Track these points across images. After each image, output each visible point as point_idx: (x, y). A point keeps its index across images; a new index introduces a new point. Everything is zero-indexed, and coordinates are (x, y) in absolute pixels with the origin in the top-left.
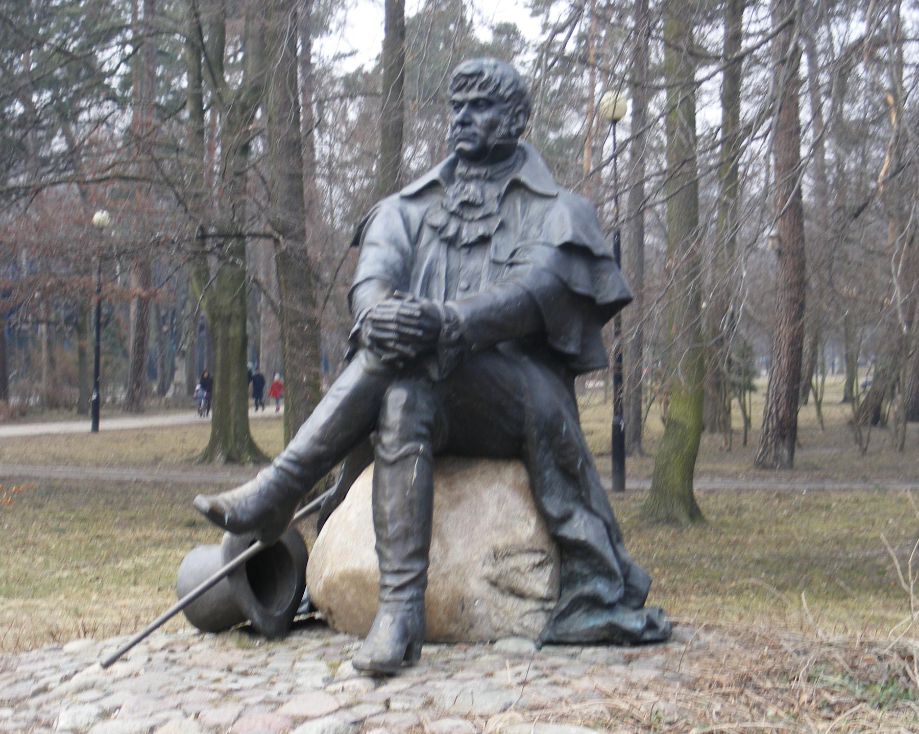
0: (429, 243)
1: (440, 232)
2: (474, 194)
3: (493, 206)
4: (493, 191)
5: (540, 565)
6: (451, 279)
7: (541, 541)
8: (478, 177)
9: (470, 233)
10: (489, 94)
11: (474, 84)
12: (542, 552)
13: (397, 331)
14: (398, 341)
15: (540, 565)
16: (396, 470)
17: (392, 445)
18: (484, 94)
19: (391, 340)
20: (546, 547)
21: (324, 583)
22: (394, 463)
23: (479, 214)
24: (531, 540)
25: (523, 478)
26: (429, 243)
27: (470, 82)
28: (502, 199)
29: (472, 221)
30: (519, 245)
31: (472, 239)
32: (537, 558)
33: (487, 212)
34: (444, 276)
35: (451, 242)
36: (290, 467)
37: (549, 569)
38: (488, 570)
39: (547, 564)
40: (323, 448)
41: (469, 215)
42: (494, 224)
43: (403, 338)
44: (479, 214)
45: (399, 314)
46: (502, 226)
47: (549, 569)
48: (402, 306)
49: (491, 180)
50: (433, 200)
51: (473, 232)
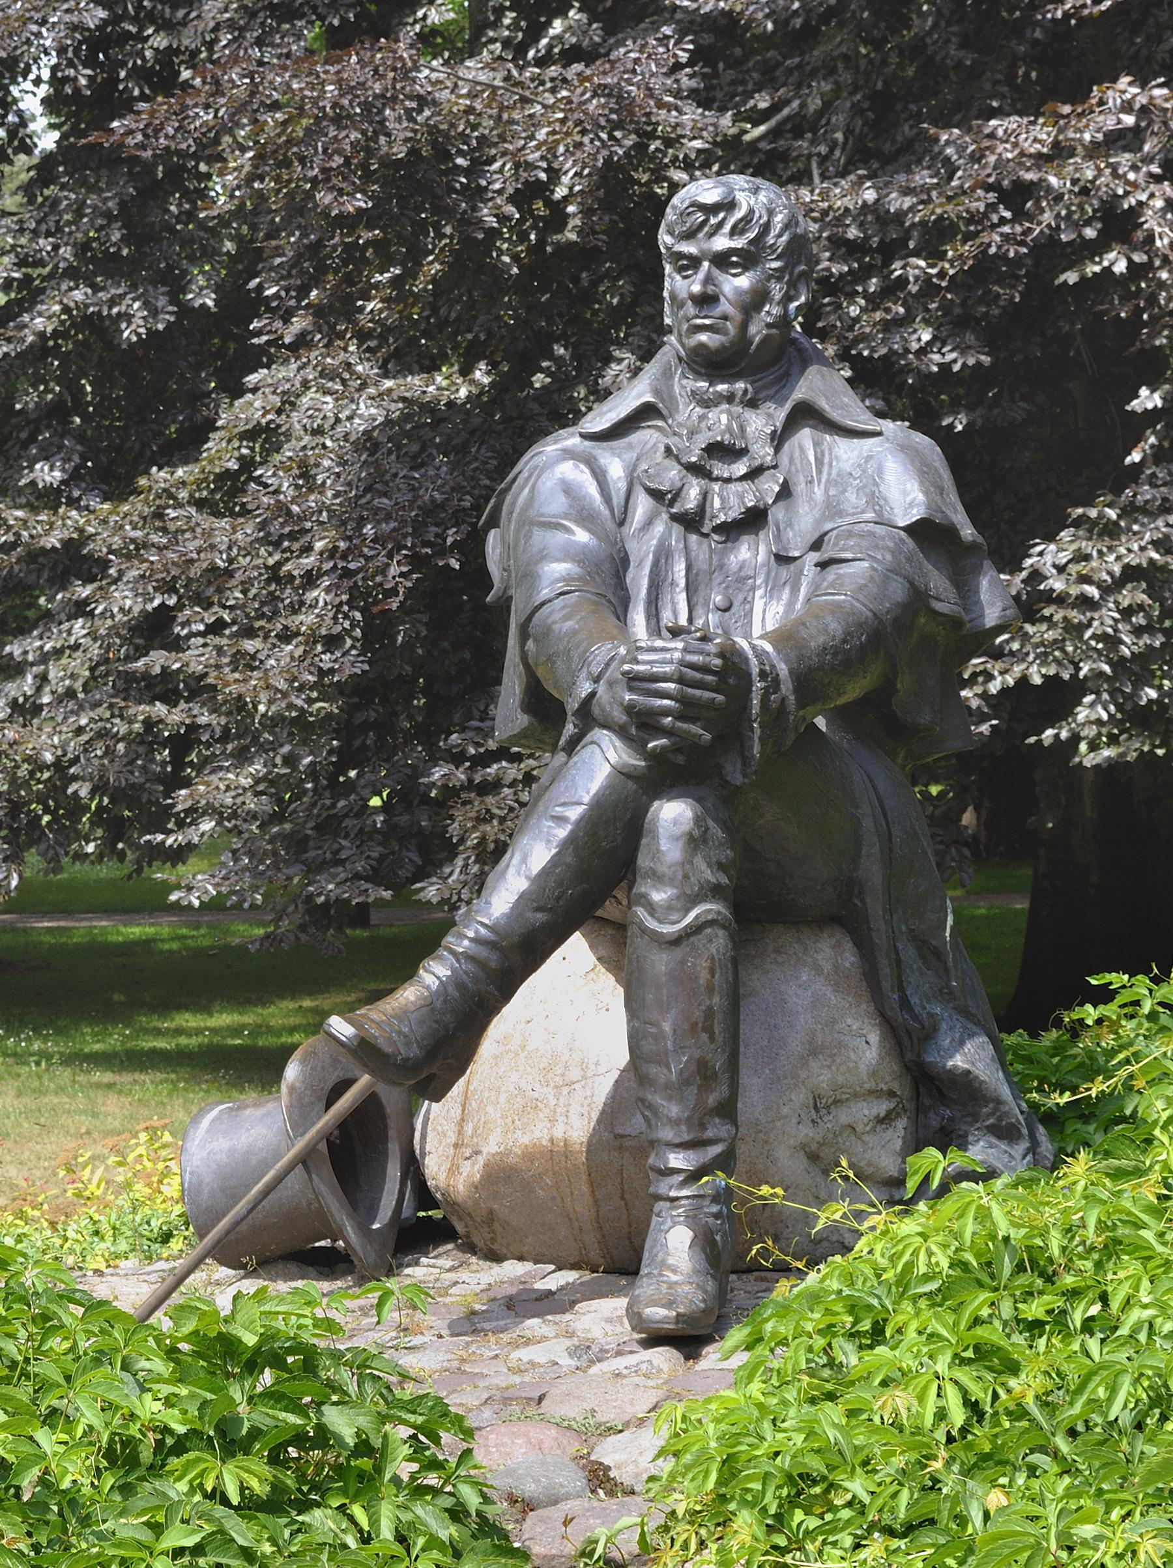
0: (649, 523)
1: (671, 504)
2: (729, 429)
3: (763, 452)
4: (759, 424)
5: (885, 1120)
6: (696, 590)
7: (891, 1077)
8: (730, 398)
9: (728, 502)
10: (751, 242)
11: (721, 225)
12: (891, 1094)
13: (680, 698)
14: (680, 717)
15: (885, 1120)
16: (678, 952)
17: (669, 908)
18: (739, 243)
19: (666, 712)
20: (896, 1086)
21: (486, 1165)
22: (676, 941)
23: (740, 468)
24: (873, 1074)
25: (849, 958)
26: (649, 523)
27: (713, 221)
28: (779, 439)
29: (728, 480)
30: (829, 526)
31: (734, 514)
32: (882, 1107)
33: (757, 463)
34: (682, 583)
35: (691, 522)
36: (483, 952)
37: (901, 1124)
38: (806, 1132)
39: (898, 1115)
40: (541, 917)
41: (720, 469)
42: (770, 486)
43: (688, 709)
44: (740, 468)
45: (683, 663)
46: (785, 492)
47: (901, 1124)
48: (685, 650)
49: (752, 404)
50: (647, 436)
51: (733, 500)
